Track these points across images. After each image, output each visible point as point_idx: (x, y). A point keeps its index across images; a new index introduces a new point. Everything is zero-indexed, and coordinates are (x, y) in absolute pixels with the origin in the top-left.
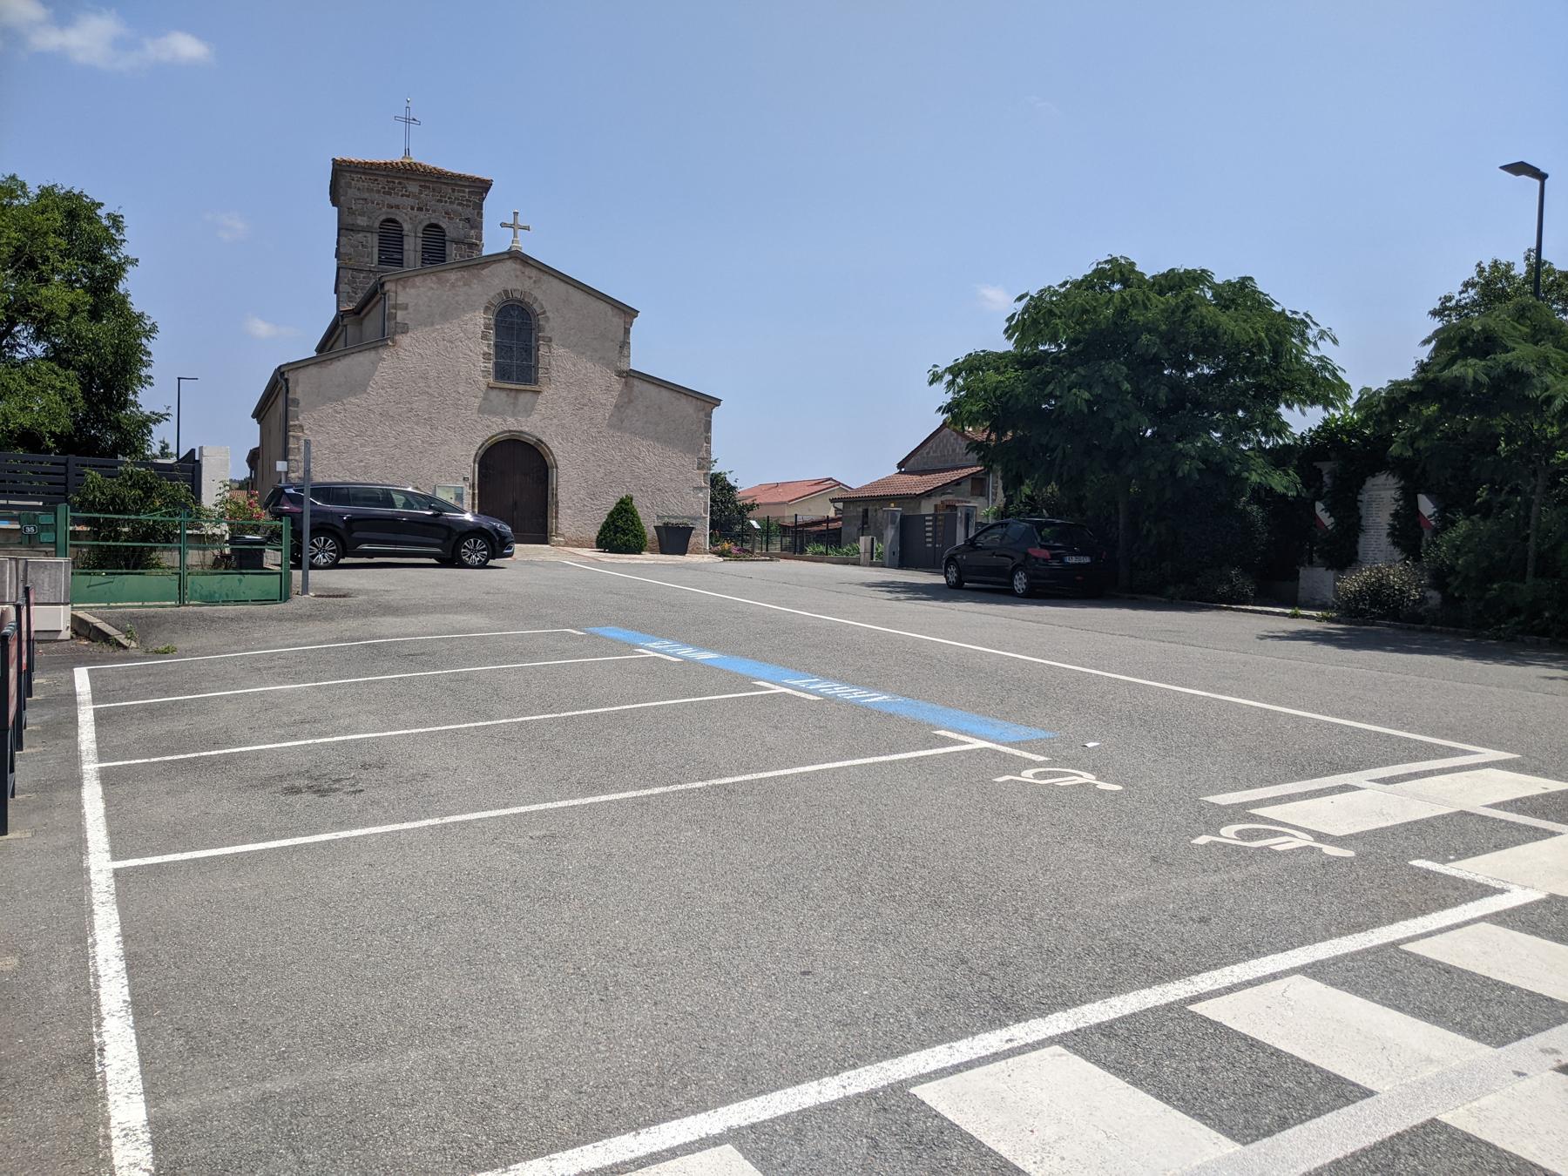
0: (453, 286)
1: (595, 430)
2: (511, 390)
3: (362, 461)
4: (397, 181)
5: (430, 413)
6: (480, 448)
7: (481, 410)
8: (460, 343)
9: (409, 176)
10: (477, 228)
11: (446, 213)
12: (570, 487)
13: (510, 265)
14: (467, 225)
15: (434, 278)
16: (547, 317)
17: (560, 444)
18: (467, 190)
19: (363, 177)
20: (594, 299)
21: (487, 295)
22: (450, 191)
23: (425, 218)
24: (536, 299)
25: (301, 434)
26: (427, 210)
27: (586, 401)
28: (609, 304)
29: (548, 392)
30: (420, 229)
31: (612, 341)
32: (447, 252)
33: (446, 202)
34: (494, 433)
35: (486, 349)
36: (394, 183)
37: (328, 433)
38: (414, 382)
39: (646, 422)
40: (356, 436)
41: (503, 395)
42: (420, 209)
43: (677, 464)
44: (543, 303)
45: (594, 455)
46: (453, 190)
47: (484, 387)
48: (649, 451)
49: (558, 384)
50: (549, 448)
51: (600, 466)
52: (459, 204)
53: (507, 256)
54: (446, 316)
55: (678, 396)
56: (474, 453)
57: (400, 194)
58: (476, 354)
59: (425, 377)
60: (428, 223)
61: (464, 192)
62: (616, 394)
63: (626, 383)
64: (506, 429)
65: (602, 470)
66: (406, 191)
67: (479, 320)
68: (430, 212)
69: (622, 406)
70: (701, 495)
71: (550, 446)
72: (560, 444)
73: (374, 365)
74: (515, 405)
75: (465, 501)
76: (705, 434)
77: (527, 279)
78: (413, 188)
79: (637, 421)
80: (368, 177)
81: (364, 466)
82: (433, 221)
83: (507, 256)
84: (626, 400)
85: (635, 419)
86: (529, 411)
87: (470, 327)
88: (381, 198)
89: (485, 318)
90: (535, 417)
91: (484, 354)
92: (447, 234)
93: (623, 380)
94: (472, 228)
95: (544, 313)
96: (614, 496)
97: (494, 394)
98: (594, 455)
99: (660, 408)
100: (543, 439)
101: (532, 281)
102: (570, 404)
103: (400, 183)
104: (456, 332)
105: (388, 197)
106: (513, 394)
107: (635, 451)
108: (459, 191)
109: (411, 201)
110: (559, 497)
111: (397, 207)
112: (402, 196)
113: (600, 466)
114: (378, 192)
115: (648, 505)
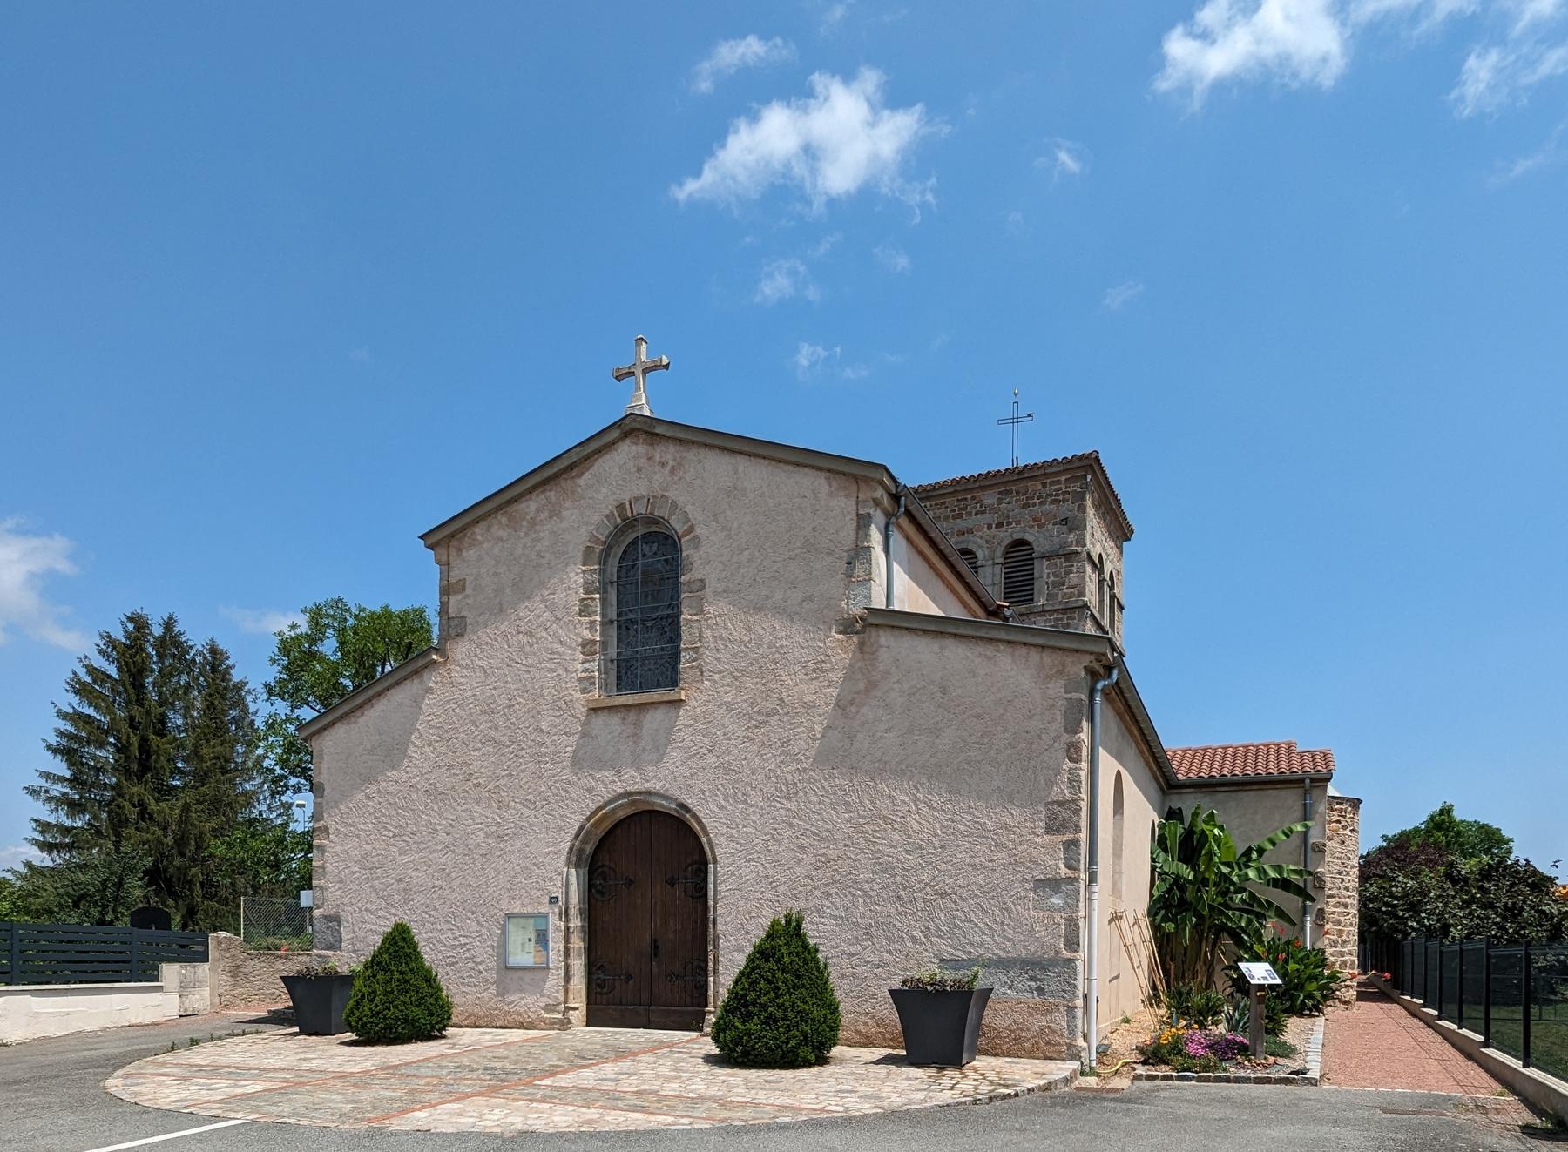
0: (533, 523)
1: (793, 766)
2: (628, 707)
3: (400, 880)
4: (969, 496)
5: (497, 778)
6: (577, 836)
7: (578, 762)
8: (544, 633)
9: (982, 484)
10: (1077, 528)
11: (1034, 520)
12: (742, 903)
13: (628, 451)
14: (1065, 528)
15: (504, 520)
16: (696, 537)
17: (722, 808)
18: (1063, 478)
19: (928, 504)
20: (791, 468)
21: (587, 523)
22: (1040, 487)
23: (1005, 536)
24: (674, 505)
25: (326, 842)
26: (1009, 523)
27: (772, 704)
28: (820, 469)
29: (696, 696)
30: (999, 551)
31: (831, 553)
32: (1036, 574)
33: (1034, 505)
34: (600, 801)
35: (587, 634)
36: (966, 499)
37: (358, 836)
38: (473, 722)
39: (910, 731)
40: (394, 836)
41: (615, 720)
42: (1000, 525)
43: (990, 825)
44: (689, 508)
45: (791, 825)
46: (1044, 485)
47: (581, 711)
48: (916, 800)
49: (717, 677)
50: (700, 822)
51: (802, 848)
52: (1052, 502)
53: (616, 434)
54: (523, 592)
55: (989, 650)
56: (566, 847)
57: (974, 512)
58: (570, 648)
59: (488, 711)
60: (1010, 539)
61: (1059, 482)
62: (837, 676)
63: (861, 645)
64: (620, 791)
65: (807, 859)
66: (981, 507)
67: (575, 580)
68: (1014, 525)
69: (852, 703)
70: (1056, 901)
71: (701, 815)
72: (722, 808)
73: (417, 703)
74: (636, 736)
75: (551, 944)
76: (1066, 737)
77: (657, 468)
78: (990, 498)
79: (888, 730)
80: (933, 503)
81: (405, 890)
82: (1016, 536)
83: (616, 434)
84: (862, 686)
85: (883, 727)
86: (660, 752)
87: (560, 597)
88: (951, 525)
89: (584, 572)
90: (674, 756)
91: (583, 646)
92: (1036, 549)
93: (855, 638)
94: (1071, 530)
95: (691, 529)
96: (835, 918)
97: (599, 720)
98: (791, 825)
99: (944, 691)
100: (689, 802)
101: (668, 469)
102: (741, 715)
103: (973, 498)
104: (537, 612)
105: (959, 521)
106: (632, 716)
107: (884, 805)
108: (1052, 483)
109: (988, 518)
110: (719, 927)
111: (970, 531)
112: (976, 514)
113: (802, 848)
114: (946, 518)
115: (917, 934)
